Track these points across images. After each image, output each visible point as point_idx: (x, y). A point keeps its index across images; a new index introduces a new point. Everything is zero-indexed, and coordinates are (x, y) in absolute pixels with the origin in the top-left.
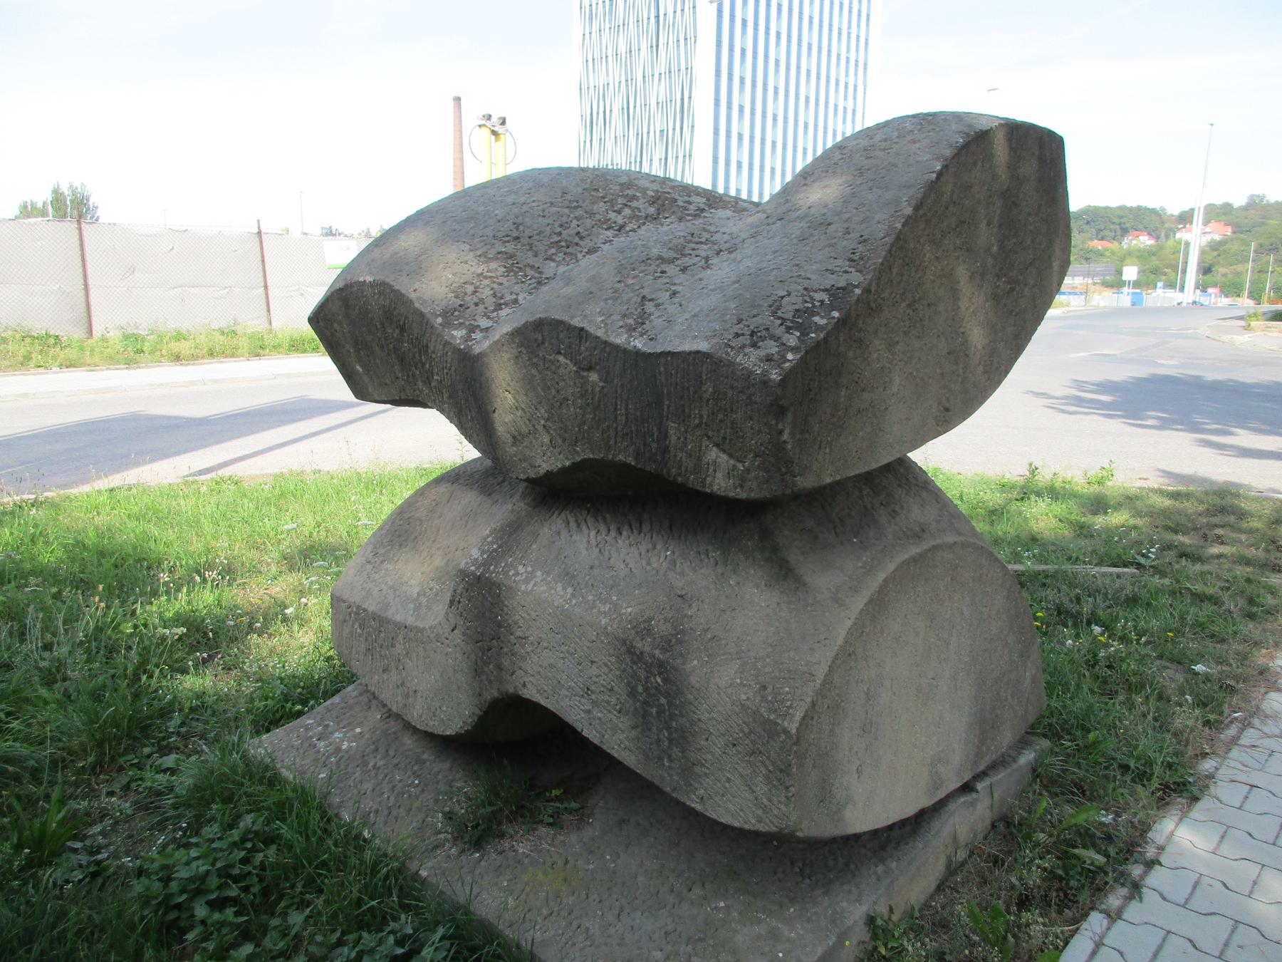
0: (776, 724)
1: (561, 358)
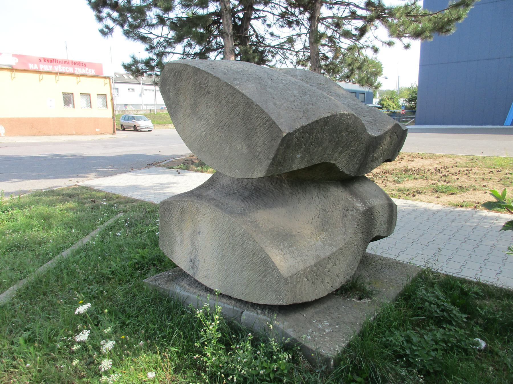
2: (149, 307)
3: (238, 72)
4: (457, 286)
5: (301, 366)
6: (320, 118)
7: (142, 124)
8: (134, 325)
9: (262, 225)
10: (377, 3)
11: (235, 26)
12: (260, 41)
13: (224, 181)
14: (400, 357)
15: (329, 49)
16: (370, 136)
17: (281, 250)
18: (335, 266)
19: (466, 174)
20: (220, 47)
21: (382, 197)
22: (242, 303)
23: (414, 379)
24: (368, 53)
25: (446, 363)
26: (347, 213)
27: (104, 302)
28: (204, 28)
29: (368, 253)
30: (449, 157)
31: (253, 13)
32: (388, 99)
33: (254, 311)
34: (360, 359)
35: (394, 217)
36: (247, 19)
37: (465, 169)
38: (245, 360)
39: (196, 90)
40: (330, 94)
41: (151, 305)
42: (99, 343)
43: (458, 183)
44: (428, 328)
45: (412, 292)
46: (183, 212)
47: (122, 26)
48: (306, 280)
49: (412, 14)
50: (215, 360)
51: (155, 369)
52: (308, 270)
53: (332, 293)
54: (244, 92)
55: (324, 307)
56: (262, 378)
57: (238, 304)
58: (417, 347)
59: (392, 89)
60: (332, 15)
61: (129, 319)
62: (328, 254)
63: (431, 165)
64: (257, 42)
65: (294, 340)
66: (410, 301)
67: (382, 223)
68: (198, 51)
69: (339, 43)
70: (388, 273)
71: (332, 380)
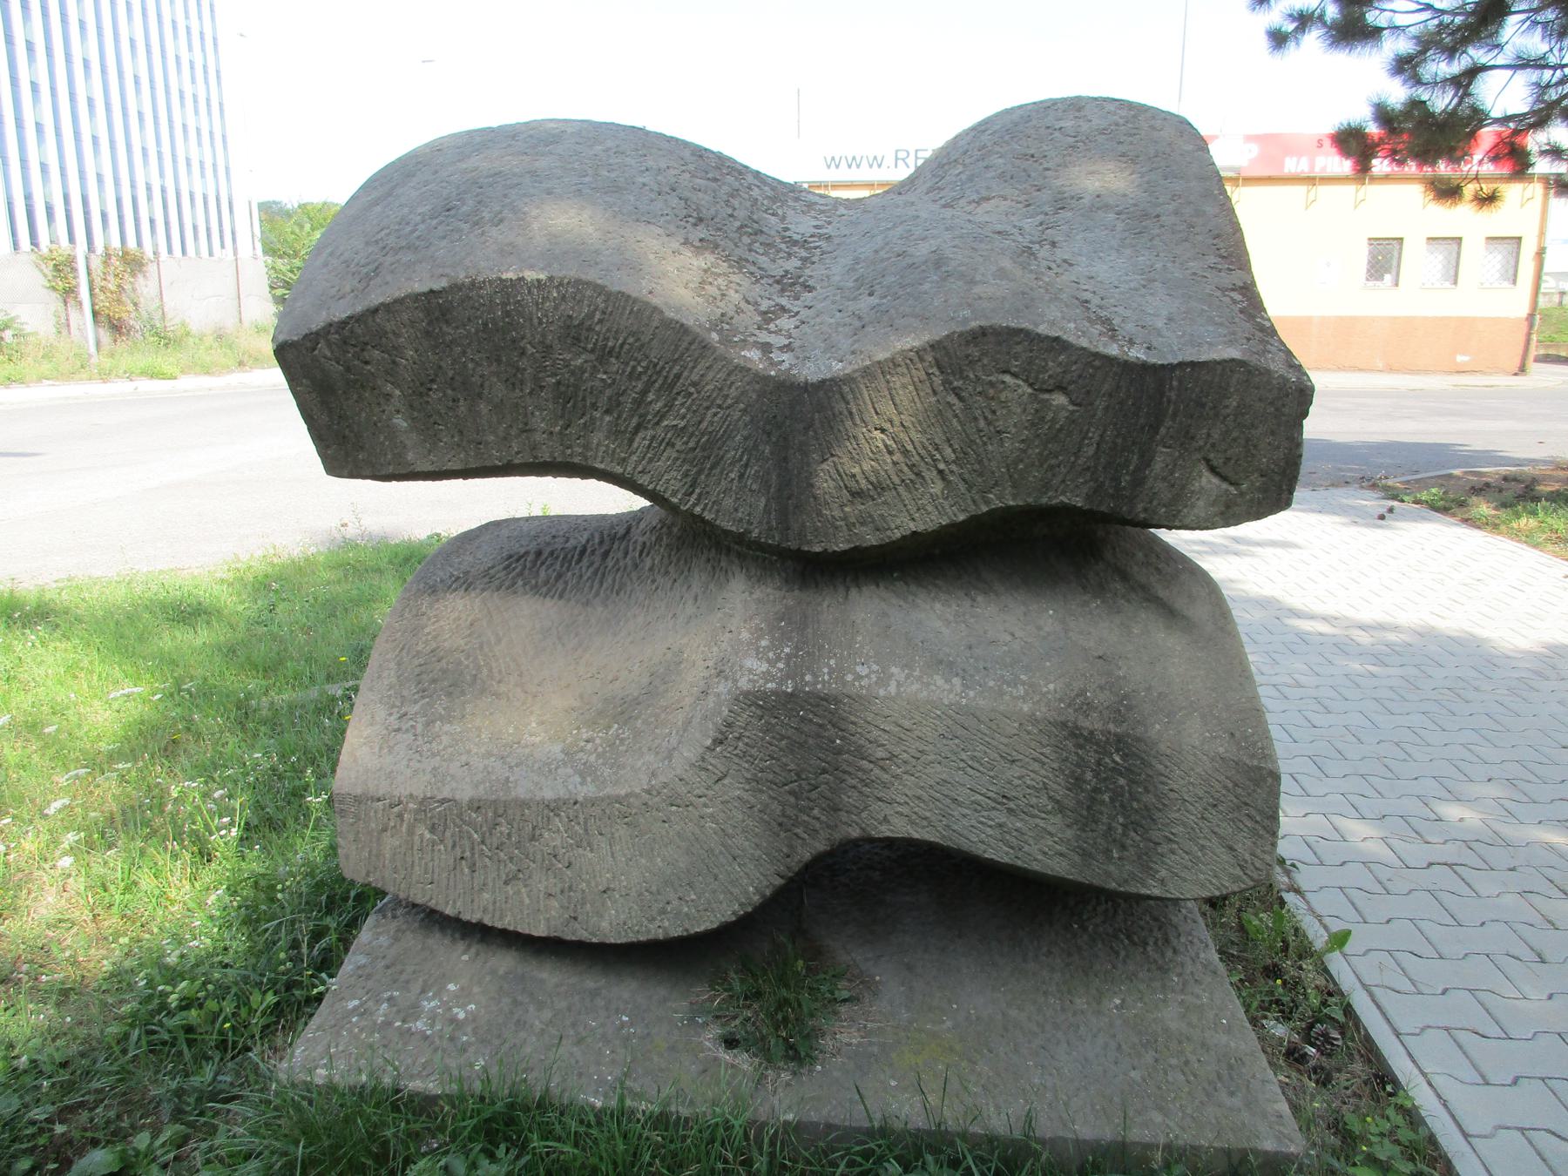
0: (1260, 768)
1: (1007, 378)
18: (590, 855)
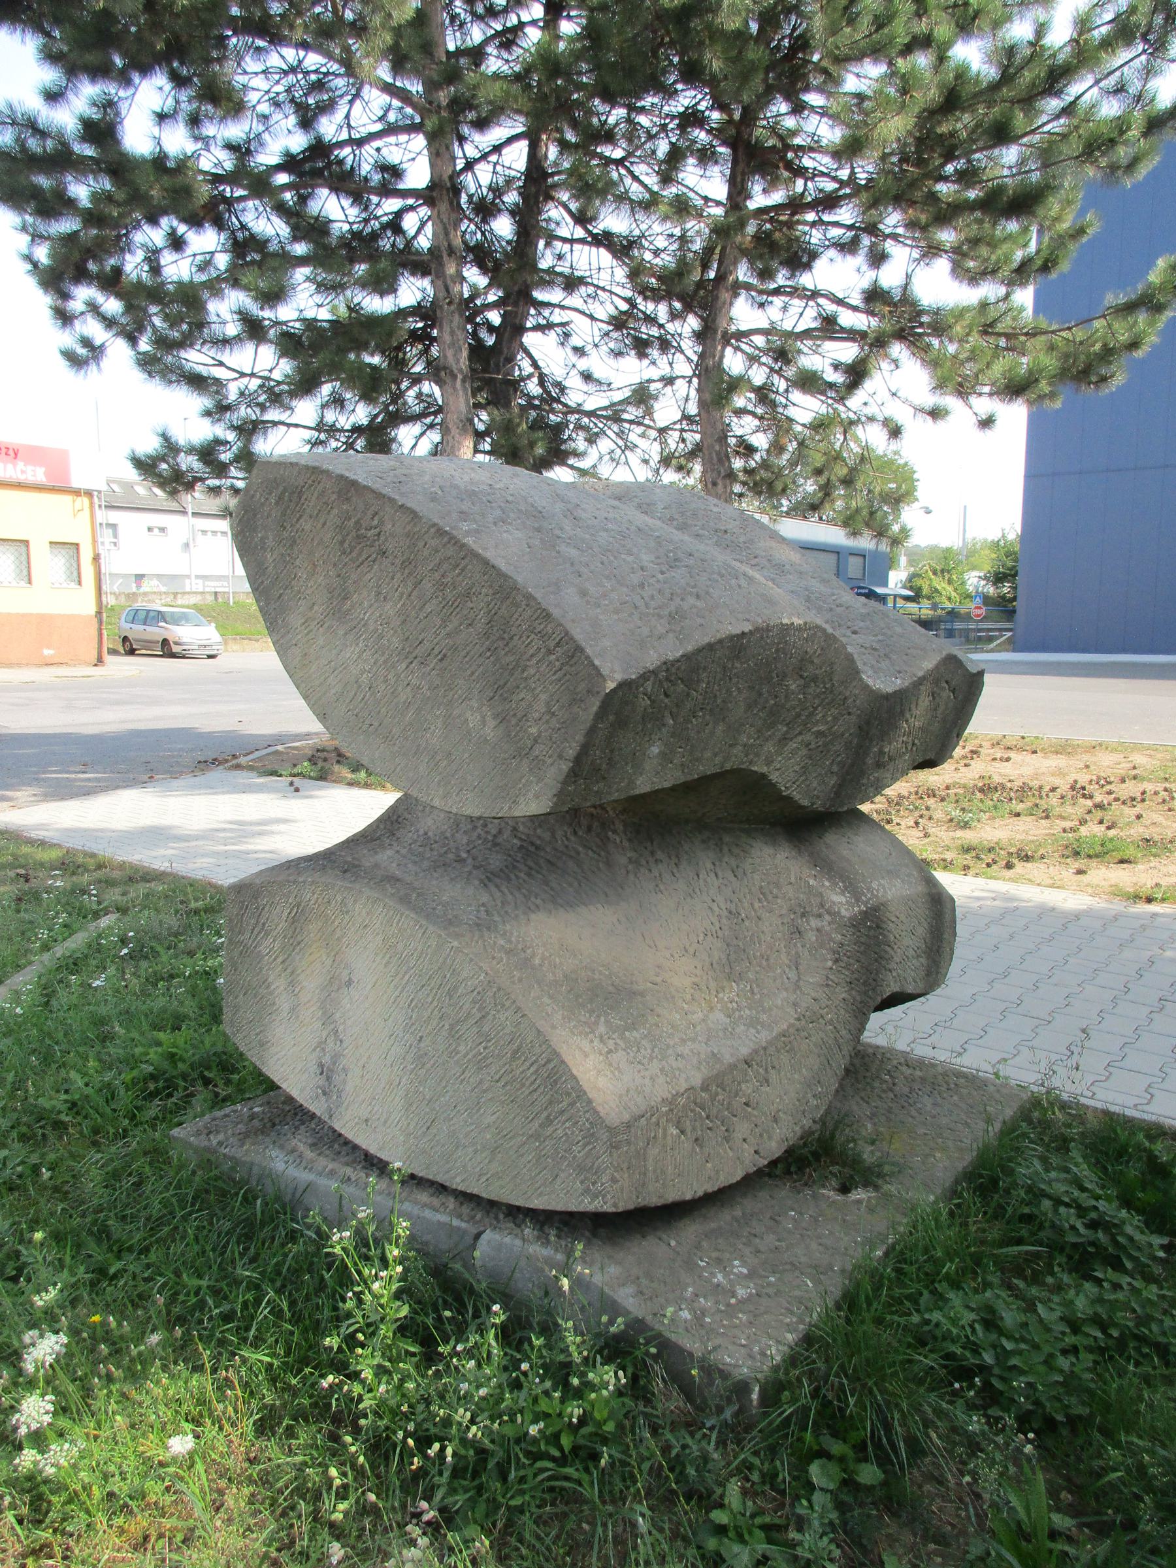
2: (184, 1218)
3: (474, 493)
4: (1139, 1147)
5: (660, 1406)
6: (719, 636)
7: (187, 634)
8: (134, 1278)
9: (543, 958)
10: (897, 295)
11: (478, 350)
12: (553, 392)
13: (430, 822)
14: (965, 1374)
15: (757, 422)
16: (872, 691)
17: (601, 1037)
19: (1164, 801)
20: (429, 411)
21: (909, 875)
22: (479, 1204)
23: (1007, 1444)
24: (874, 437)
25: (1104, 1391)
26: (802, 923)
27: (42, 1201)
28: (383, 353)
29: (870, 1045)
30: (1114, 750)
31: (532, 311)
32: (935, 573)
33: (517, 1231)
34: (842, 1384)
35: (946, 936)
36: (513, 329)
37: (1160, 787)
38: (483, 1392)
39: (346, 545)
40: (754, 562)
41: (190, 1214)
42: (20, 1340)
43: (1141, 830)
44: (1050, 1280)
45: (1003, 1167)
46: (297, 918)
47: (132, 340)
48: (675, 1132)
49: (1000, 328)
50: (387, 1391)
51: (197, 1421)
52: (682, 1101)
53: (760, 1173)
54: (489, 555)
55: (733, 1217)
56: (534, 1450)
57: (465, 1210)
58: (1016, 1341)
59: (944, 544)
60: (765, 325)
61: (119, 1258)
62: (744, 1051)
63: (1060, 773)
64: (542, 400)
65: (637, 1325)
66: (996, 1196)
67: (911, 953)
68: (365, 422)
69: (785, 406)
70: (929, 1107)
71: (756, 1453)
